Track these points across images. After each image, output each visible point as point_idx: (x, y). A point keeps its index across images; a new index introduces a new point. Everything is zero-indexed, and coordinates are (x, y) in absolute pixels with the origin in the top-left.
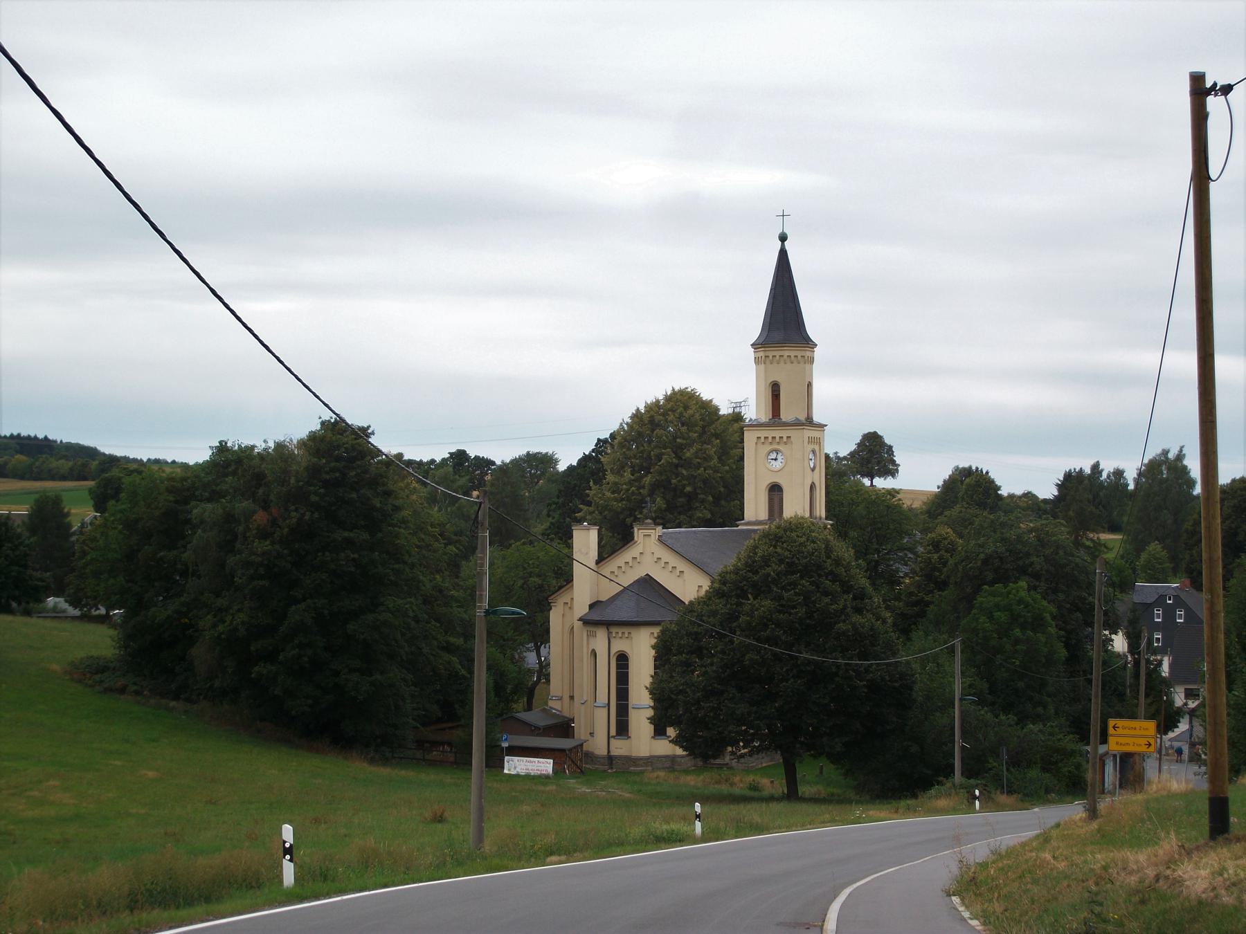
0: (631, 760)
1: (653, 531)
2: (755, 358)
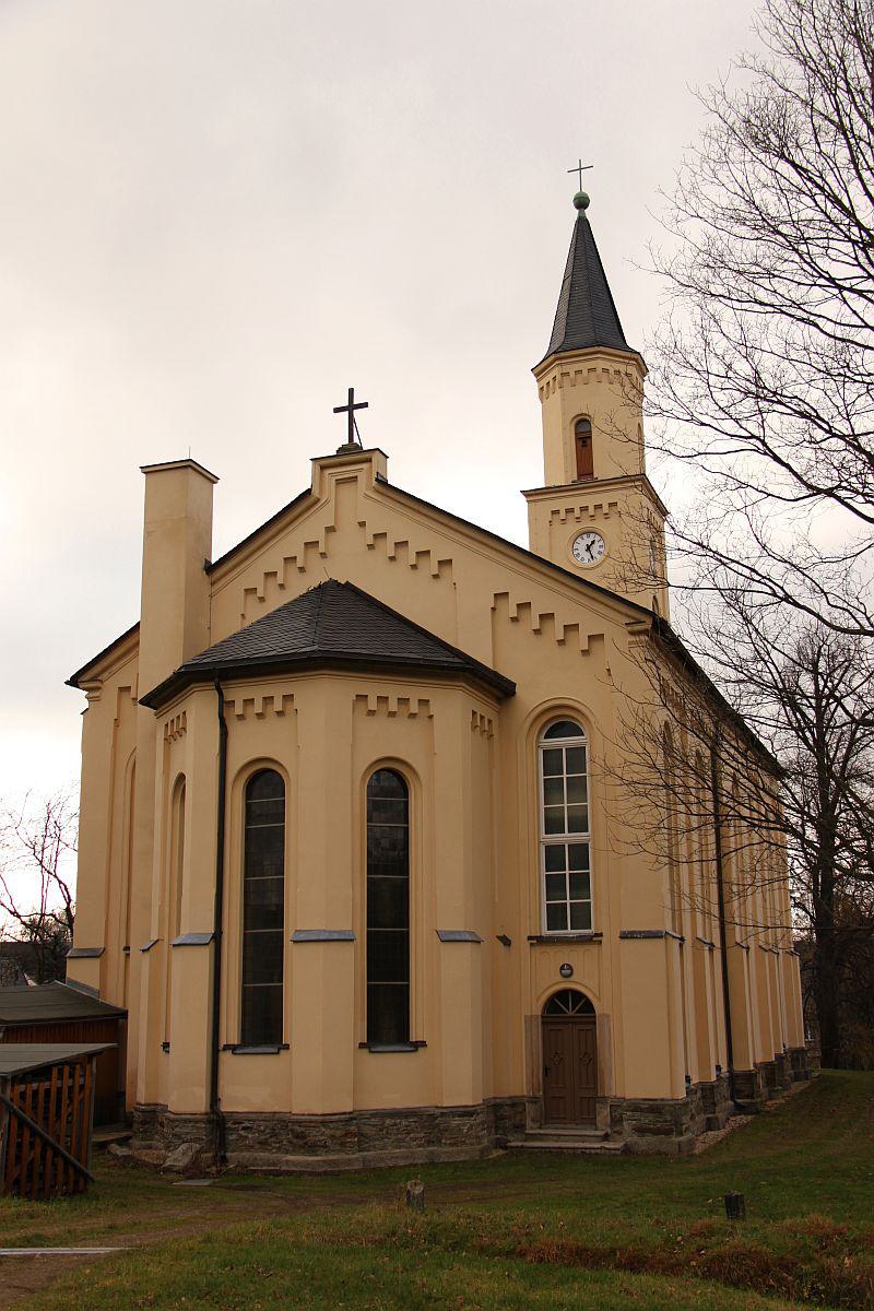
0: (287, 1130)
1: (364, 466)
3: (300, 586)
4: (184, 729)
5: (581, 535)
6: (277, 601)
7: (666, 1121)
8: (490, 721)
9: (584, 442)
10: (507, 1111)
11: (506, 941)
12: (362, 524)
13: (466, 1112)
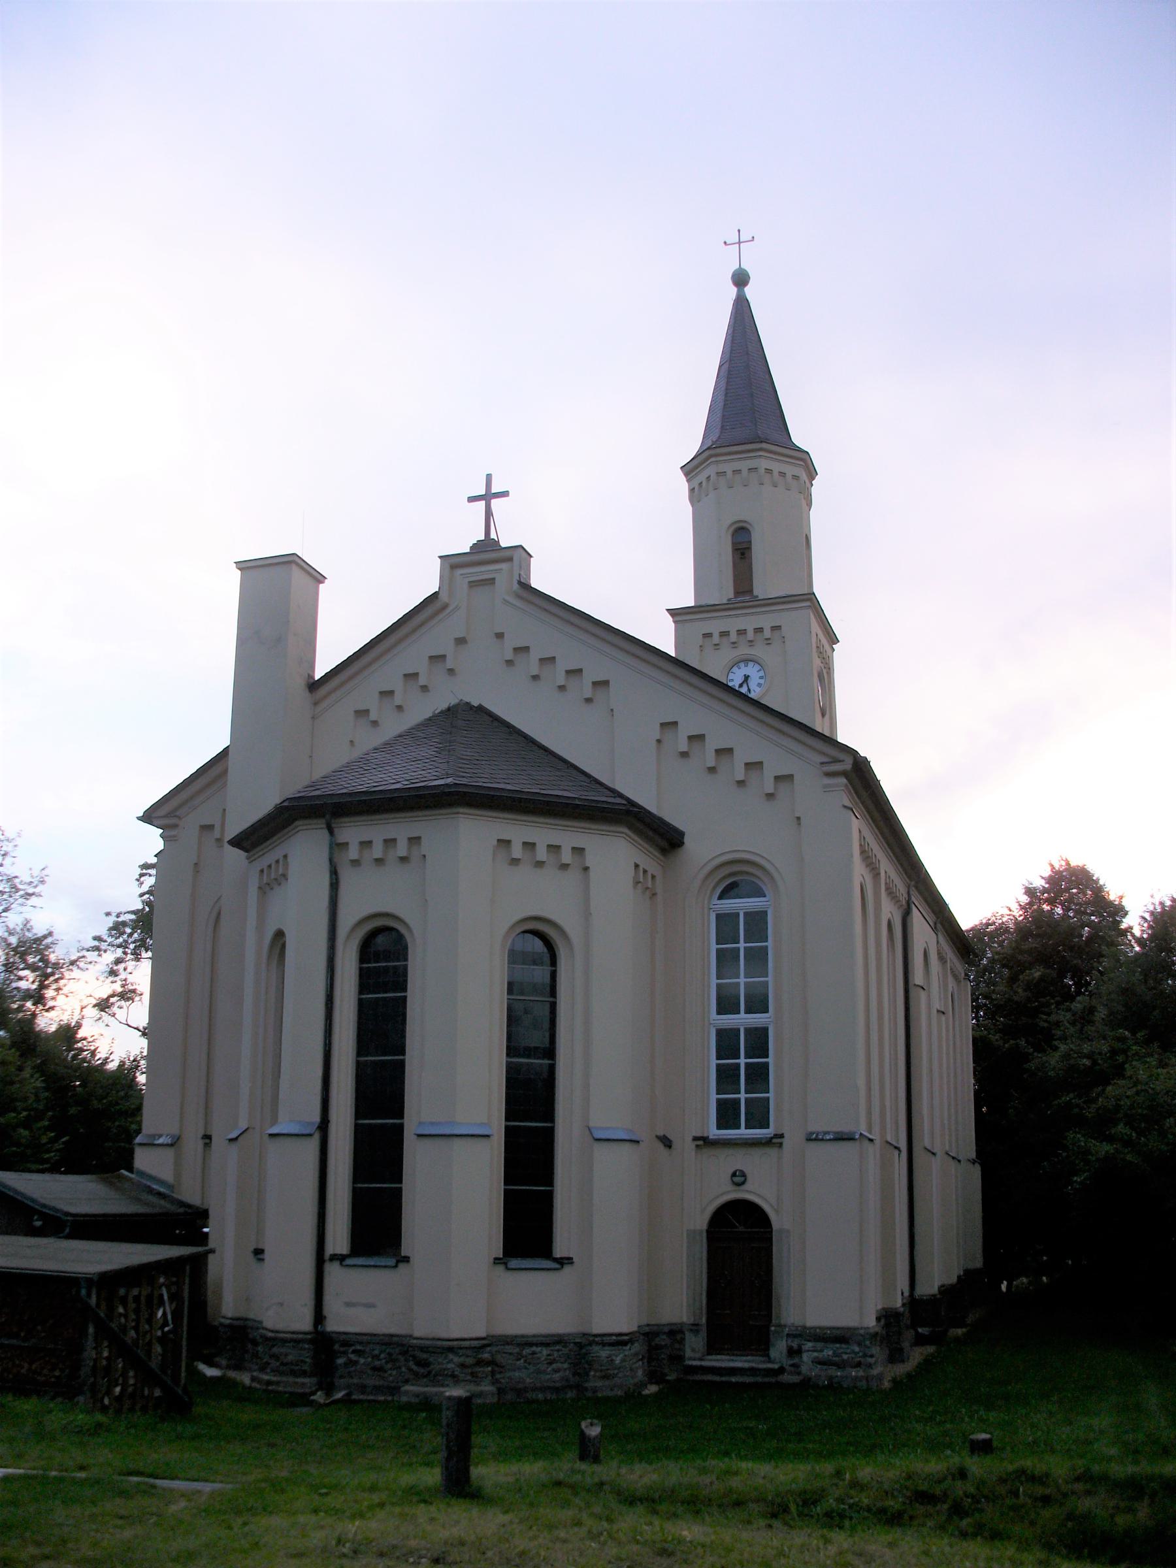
1: (504, 566)
2: (692, 490)
3: (422, 709)
4: (284, 876)
5: (736, 664)
6: (393, 726)
7: (853, 1352)
8: (653, 877)
9: (743, 554)
10: (663, 1340)
11: (666, 1142)
12: (500, 636)
13: (619, 1341)
